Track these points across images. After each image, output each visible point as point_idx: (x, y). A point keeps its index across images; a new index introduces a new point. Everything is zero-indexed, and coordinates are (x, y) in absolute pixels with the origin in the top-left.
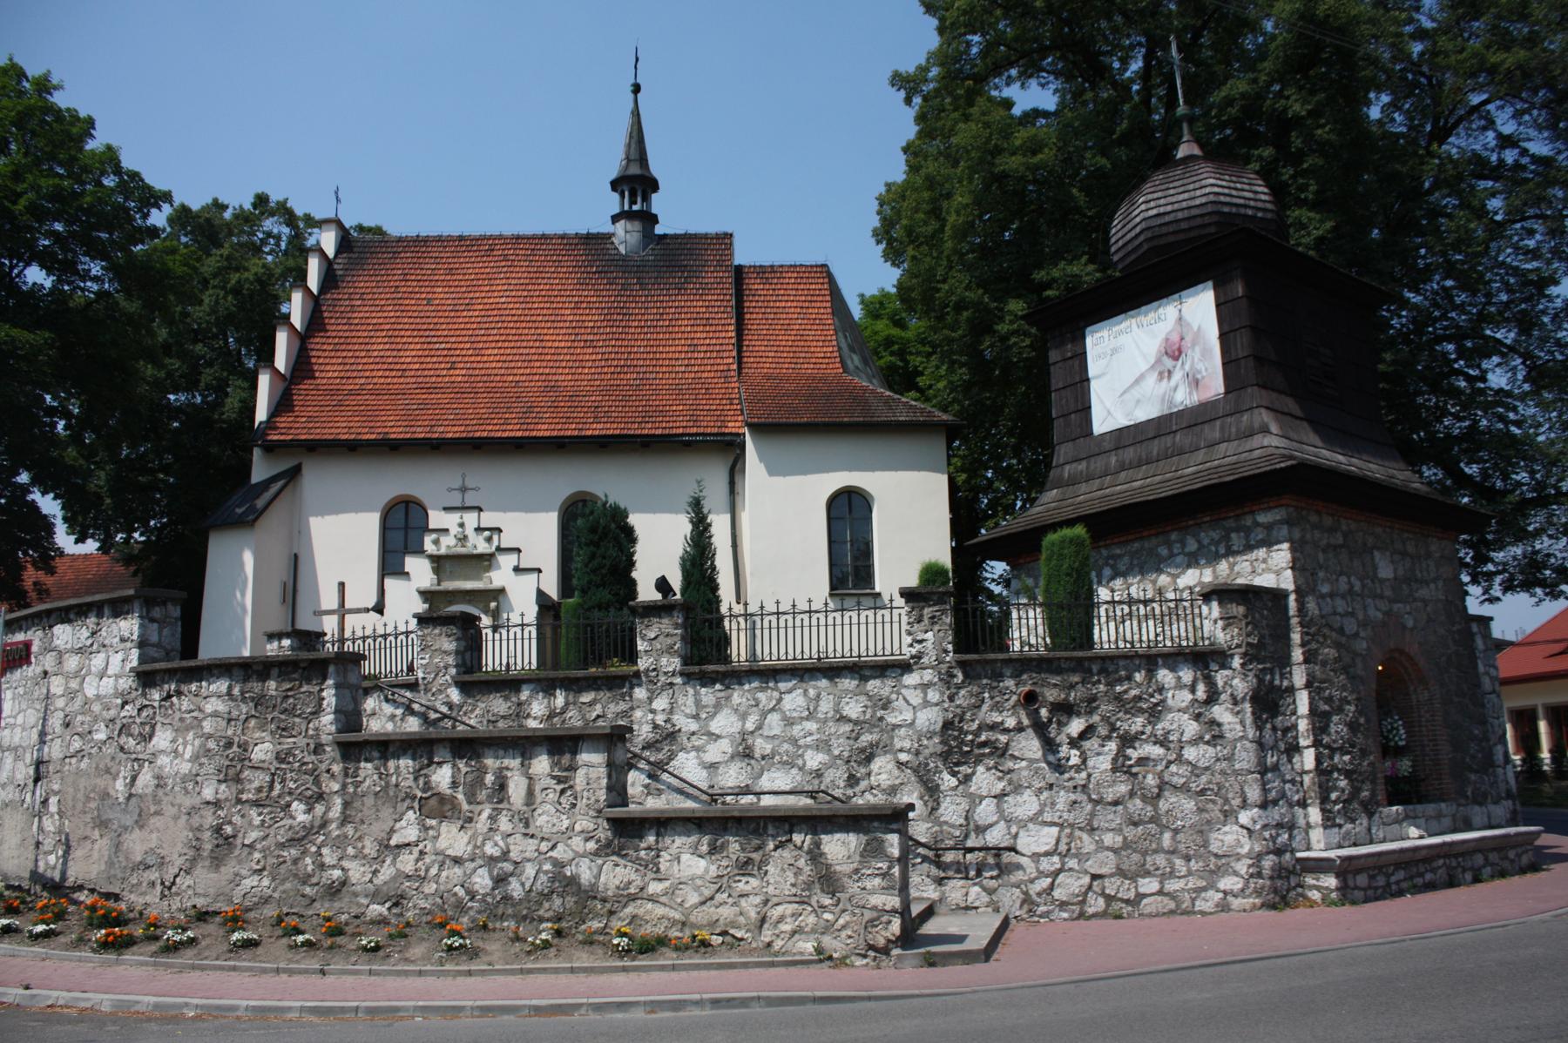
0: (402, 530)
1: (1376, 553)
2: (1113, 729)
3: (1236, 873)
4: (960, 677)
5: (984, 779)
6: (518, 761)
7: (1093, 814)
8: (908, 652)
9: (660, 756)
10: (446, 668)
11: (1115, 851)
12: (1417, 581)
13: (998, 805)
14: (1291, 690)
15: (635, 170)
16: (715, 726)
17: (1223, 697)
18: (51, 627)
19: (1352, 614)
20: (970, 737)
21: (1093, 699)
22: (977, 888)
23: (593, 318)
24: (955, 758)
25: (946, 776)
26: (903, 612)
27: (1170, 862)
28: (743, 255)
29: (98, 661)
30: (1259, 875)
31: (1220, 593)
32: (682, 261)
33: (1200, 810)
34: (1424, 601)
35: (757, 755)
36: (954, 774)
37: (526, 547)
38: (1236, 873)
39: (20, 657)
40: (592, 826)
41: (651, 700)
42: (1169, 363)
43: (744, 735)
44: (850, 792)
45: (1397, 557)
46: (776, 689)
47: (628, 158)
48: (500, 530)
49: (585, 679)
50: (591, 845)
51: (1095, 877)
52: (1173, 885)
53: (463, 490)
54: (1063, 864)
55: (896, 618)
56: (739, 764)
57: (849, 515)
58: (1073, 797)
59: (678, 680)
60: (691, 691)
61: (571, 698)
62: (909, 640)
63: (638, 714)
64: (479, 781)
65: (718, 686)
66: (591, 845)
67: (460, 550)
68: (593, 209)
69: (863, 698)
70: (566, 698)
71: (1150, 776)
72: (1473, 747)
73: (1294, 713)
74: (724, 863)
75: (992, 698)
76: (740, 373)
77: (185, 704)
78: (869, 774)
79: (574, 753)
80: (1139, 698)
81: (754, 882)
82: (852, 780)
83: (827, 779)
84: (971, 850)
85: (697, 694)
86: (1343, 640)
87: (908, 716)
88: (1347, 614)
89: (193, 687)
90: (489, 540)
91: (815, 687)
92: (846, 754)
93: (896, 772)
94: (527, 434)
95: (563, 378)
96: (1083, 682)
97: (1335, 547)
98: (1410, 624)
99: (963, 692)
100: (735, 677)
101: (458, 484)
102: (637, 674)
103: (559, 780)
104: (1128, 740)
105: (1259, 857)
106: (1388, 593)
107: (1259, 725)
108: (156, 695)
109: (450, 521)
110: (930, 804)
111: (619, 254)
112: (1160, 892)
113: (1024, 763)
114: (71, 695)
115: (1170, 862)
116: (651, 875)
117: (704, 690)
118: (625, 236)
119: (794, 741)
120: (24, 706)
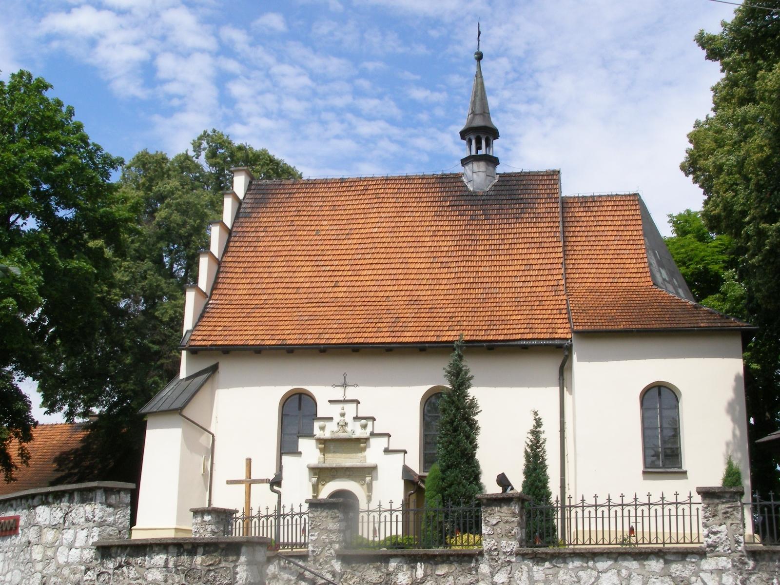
0: (297, 413)
8: (705, 542)
10: (331, 543)
15: (479, 122)
18: (34, 507)
23: (447, 244)
26: (700, 507)
28: (570, 188)
29: (68, 535)
32: (523, 194)
37: (391, 410)
39: (9, 529)
47: (473, 113)
48: (374, 419)
49: (441, 555)
55: (694, 512)
57: (659, 400)
59: (514, 559)
61: (429, 572)
62: (706, 531)
65: (547, 564)
67: (342, 435)
68: (448, 150)
70: (425, 571)
77: (132, 573)
85: (530, 570)
89: (139, 560)
90: (364, 427)
91: (627, 568)
94: (395, 340)
95: (424, 294)
99: (753, 578)
100: (564, 557)
102: (481, 554)
108: (111, 565)
109: (334, 411)
111: (467, 190)
114: (47, 560)
117: (535, 568)
118: (476, 178)
120: (12, 567)
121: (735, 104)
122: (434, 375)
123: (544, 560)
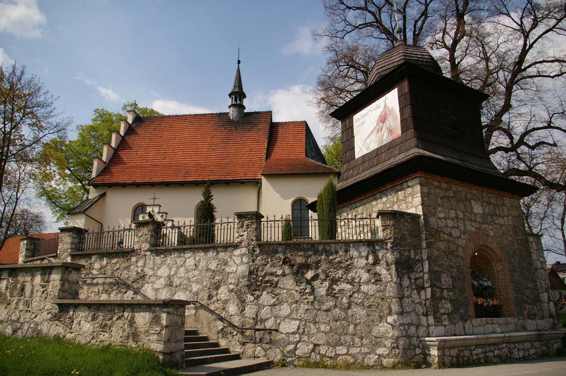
1: (472, 201)
2: (327, 276)
3: (385, 346)
4: (258, 251)
5: (266, 298)
6: (30, 278)
7: (316, 315)
9: (139, 286)
11: (326, 333)
12: (496, 216)
13: (271, 310)
14: (422, 261)
16: (159, 273)
17: (382, 262)
19: (457, 228)
20: (261, 278)
21: (320, 262)
22: (259, 348)
24: (253, 288)
25: (249, 296)
27: (352, 339)
28: (277, 118)
30: (397, 347)
31: (382, 214)
33: (368, 315)
34: (501, 226)
35: (174, 285)
36: (253, 295)
38: (385, 346)
40: (51, 307)
41: (137, 262)
42: (381, 124)
43: (169, 277)
44: (209, 302)
45: (484, 204)
46: (184, 257)
47: (235, 86)
50: (49, 316)
51: (316, 345)
52: (353, 351)
53: (154, 199)
54: (300, 339)
56: (167, 289)
58: (307, 307)
59: (149, 253)
60: (152, 258)
62: (237, 235)
63: (132, 267)
64: (15, 286)
65: (162, 256)
66: (49, 316)
68: (224, 105)
69: (216, 261)
71: (345, 298)
72: (528, 292)
73: (422, 271)
74: (96, 326)
75: (272, 261)
76: (266, 159)
78: (217, 294)
79: (50, 274)
80: (340, 262)
81: (107, 335)
82: (210, 297)
83: (200, 296)
84: (258, 330)
85: (154, 259)
86: (451, 239)
87: (234, 269)
88: (454, 227)
92: (209, 285)
93: (228, 294)
96: (315, 254)
97: (448, 197)
98: (492, 234)
101: (153, 197)
103: (43, 287)
104: (334, 281)
105: (397, 338)
106: (479, 219)
107: (400, 276)
110: (241, 308)
112: (347, 354)
113: (285, 291)
115: (352, 339)
116: (68, 330)
119: (189, 279)
121: (534, 293)
122: (196, 197)
123: (161, 253)
